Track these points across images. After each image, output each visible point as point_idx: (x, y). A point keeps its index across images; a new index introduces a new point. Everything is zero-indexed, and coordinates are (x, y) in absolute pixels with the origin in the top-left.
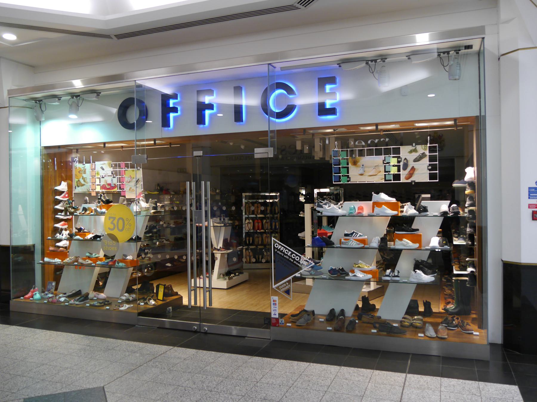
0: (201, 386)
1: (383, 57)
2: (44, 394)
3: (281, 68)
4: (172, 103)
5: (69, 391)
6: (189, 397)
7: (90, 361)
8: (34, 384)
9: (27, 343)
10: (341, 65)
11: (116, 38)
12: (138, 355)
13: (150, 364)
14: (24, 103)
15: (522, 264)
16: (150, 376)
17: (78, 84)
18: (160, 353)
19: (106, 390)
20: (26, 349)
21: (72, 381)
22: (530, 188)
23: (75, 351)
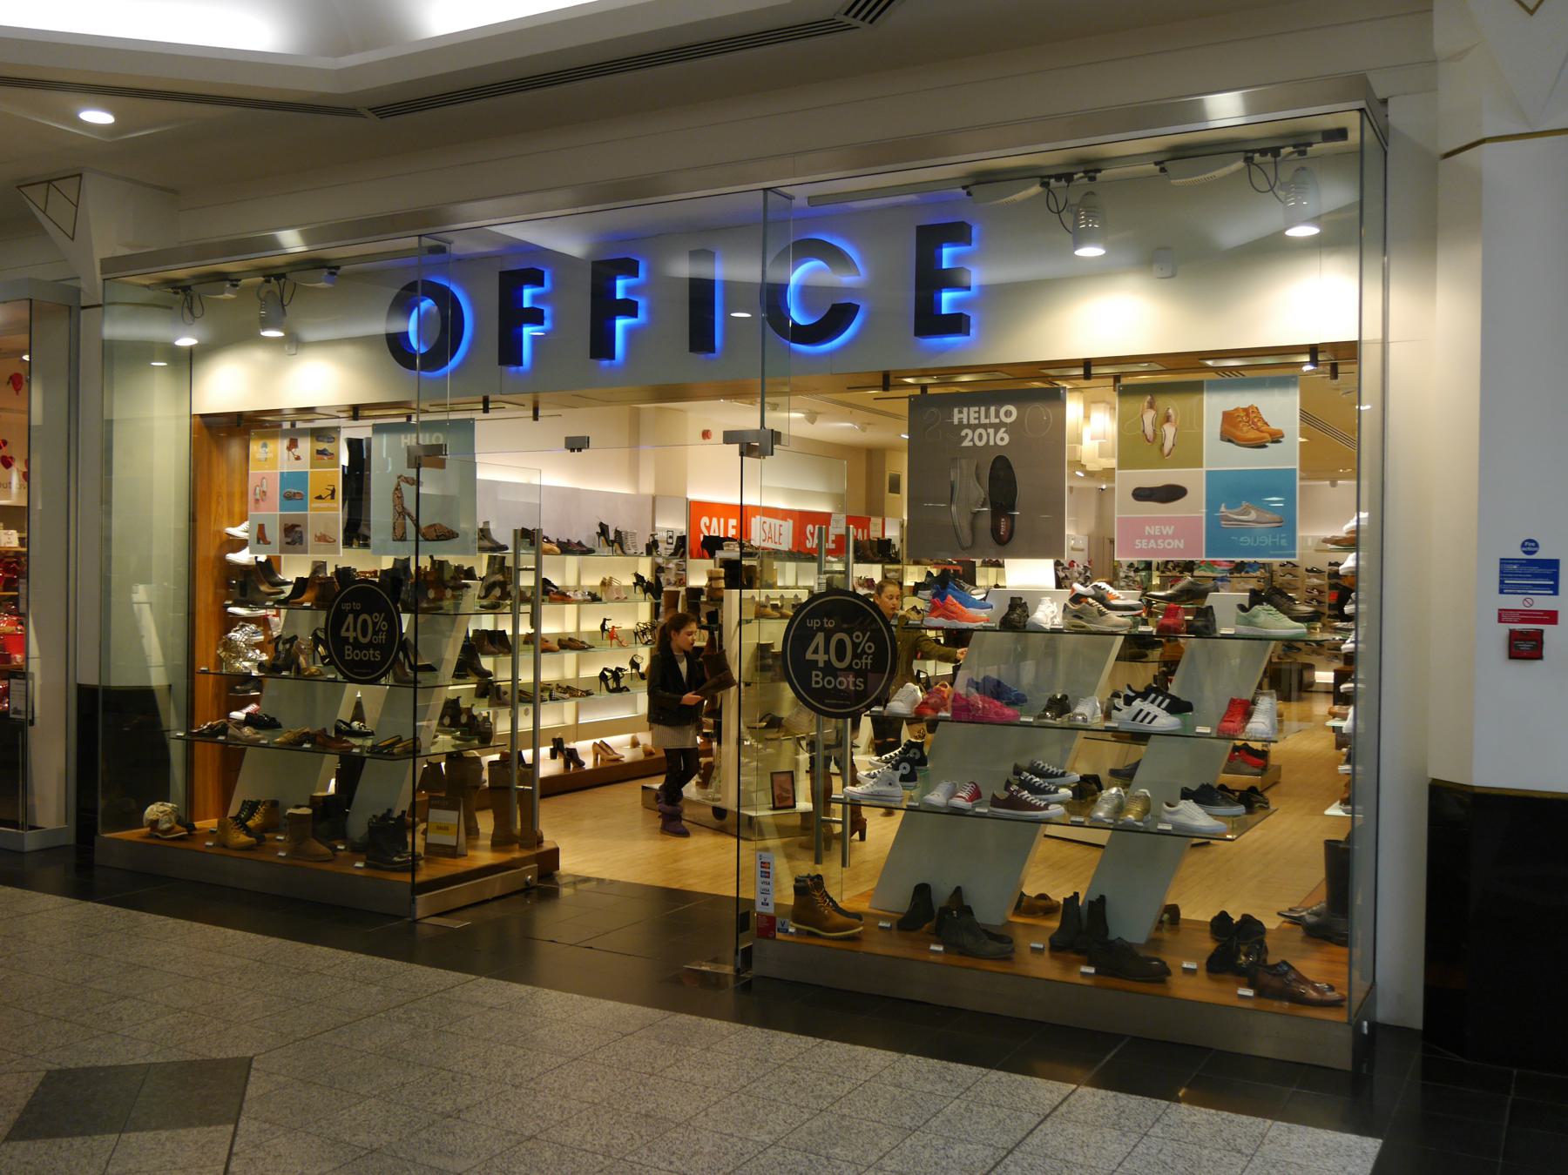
0: (500, 1073)
1: (1302, 140)
2: (100, 1064)
3: (809, 198)
4: (621, 286)
5: (165, 1061)
6: (453, 1097)
7: (247, 996)
8: (87, 1040)
9: (107, 945)
10: (972, 189)
11: (373, 115)
12: (374, 990)
13: (396, 1014)
14: (148, 295)
15: (1477, 790)
16: (381, 1041)
17: (292, 241)
18: (435, 990)
19: (254, 1065)
20: (99, 959)
21: (179, 1040)
22: (1503, 562)
23: (217, 971)
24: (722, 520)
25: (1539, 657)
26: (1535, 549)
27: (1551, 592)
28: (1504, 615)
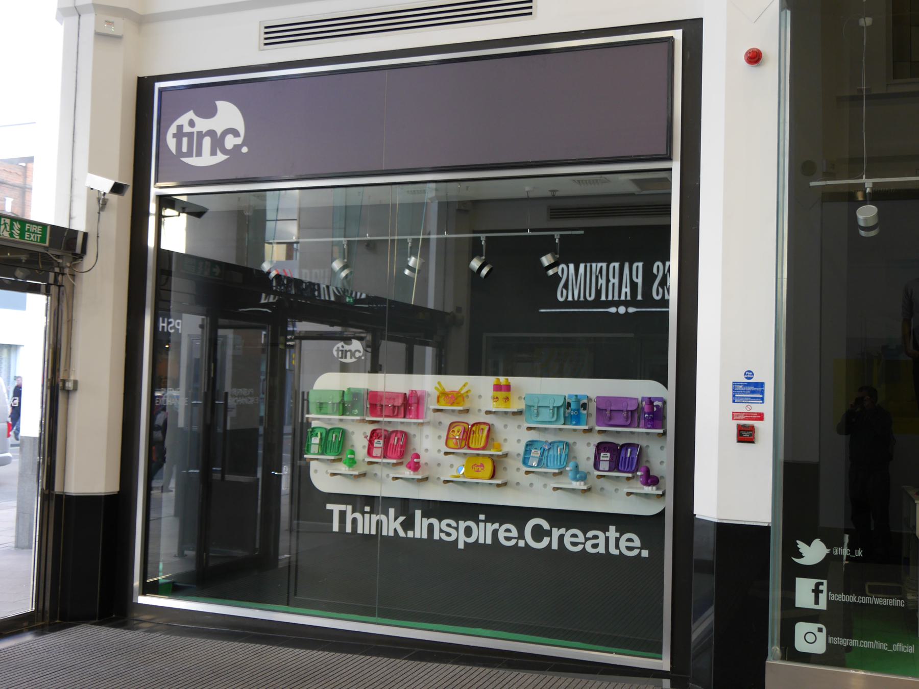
22: (735, 384)
24: (349, 529)
25: (739, 441)
27: (761, 402)
28: (735, 415)
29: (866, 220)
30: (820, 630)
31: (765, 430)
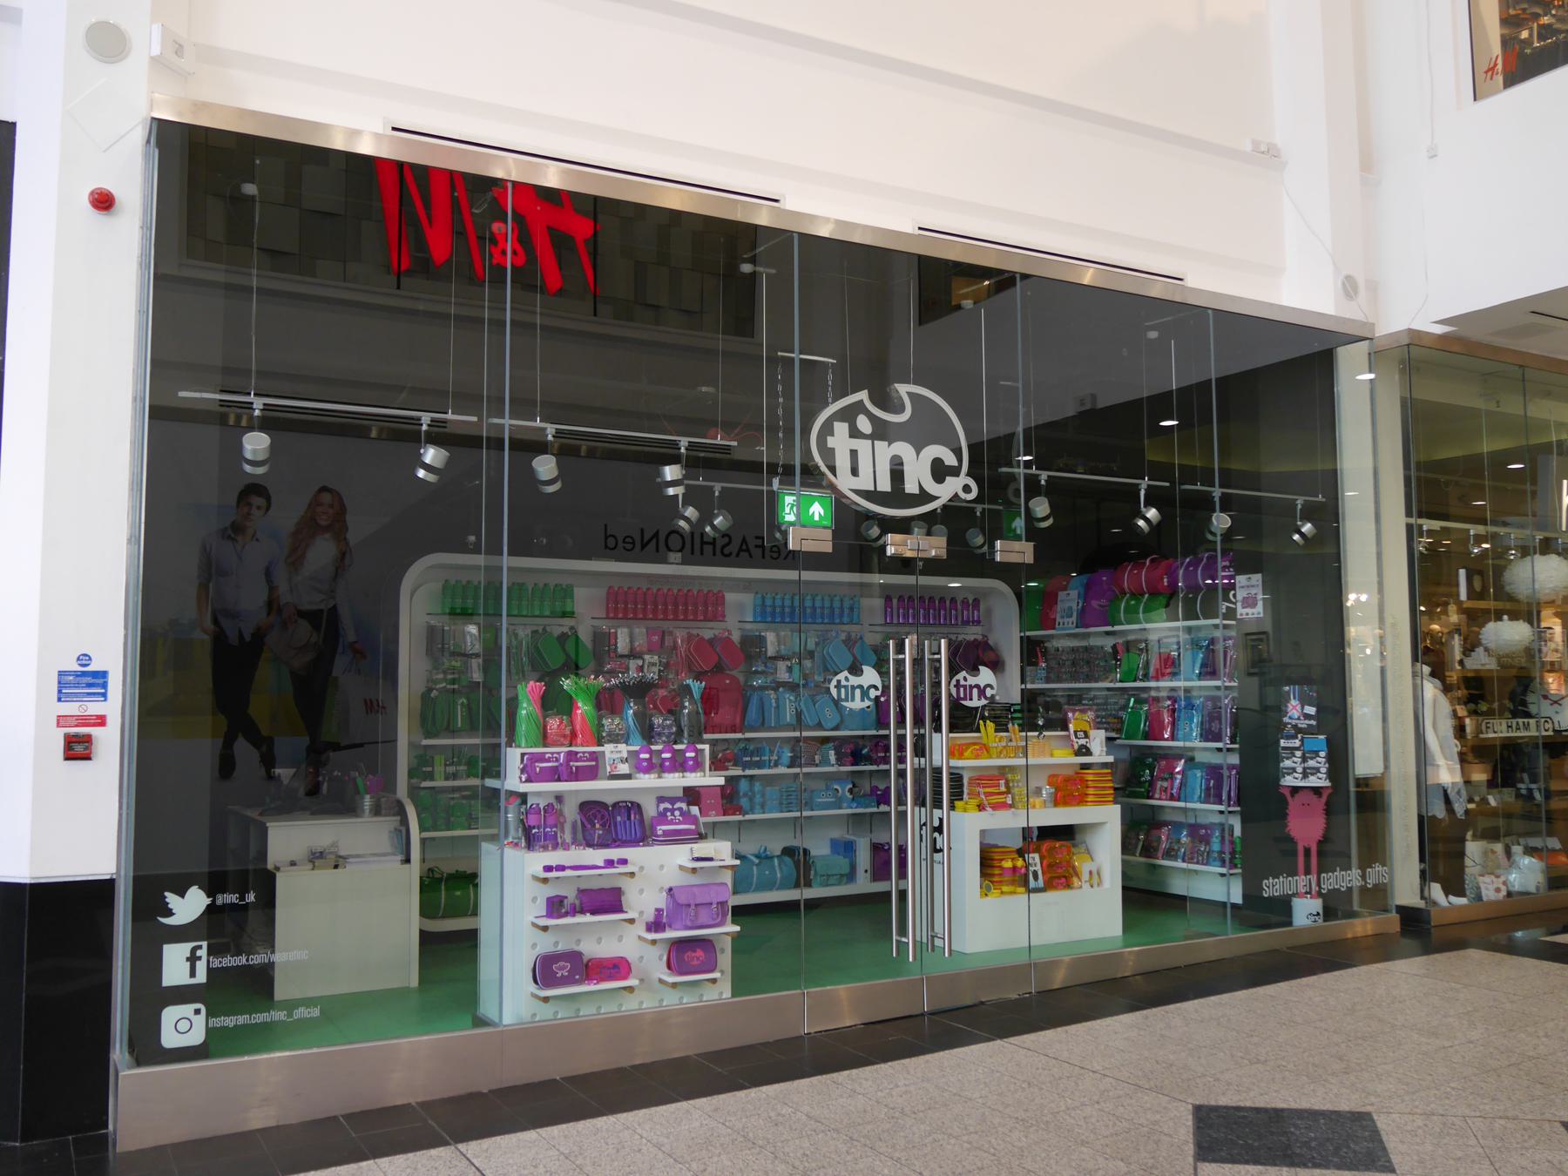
22: (61, 674)
26: (87, 662)
27: (103, 699)
28: (61, 721)
29: (254, 451)
30: (197, 1012)
31: (110, 742)
